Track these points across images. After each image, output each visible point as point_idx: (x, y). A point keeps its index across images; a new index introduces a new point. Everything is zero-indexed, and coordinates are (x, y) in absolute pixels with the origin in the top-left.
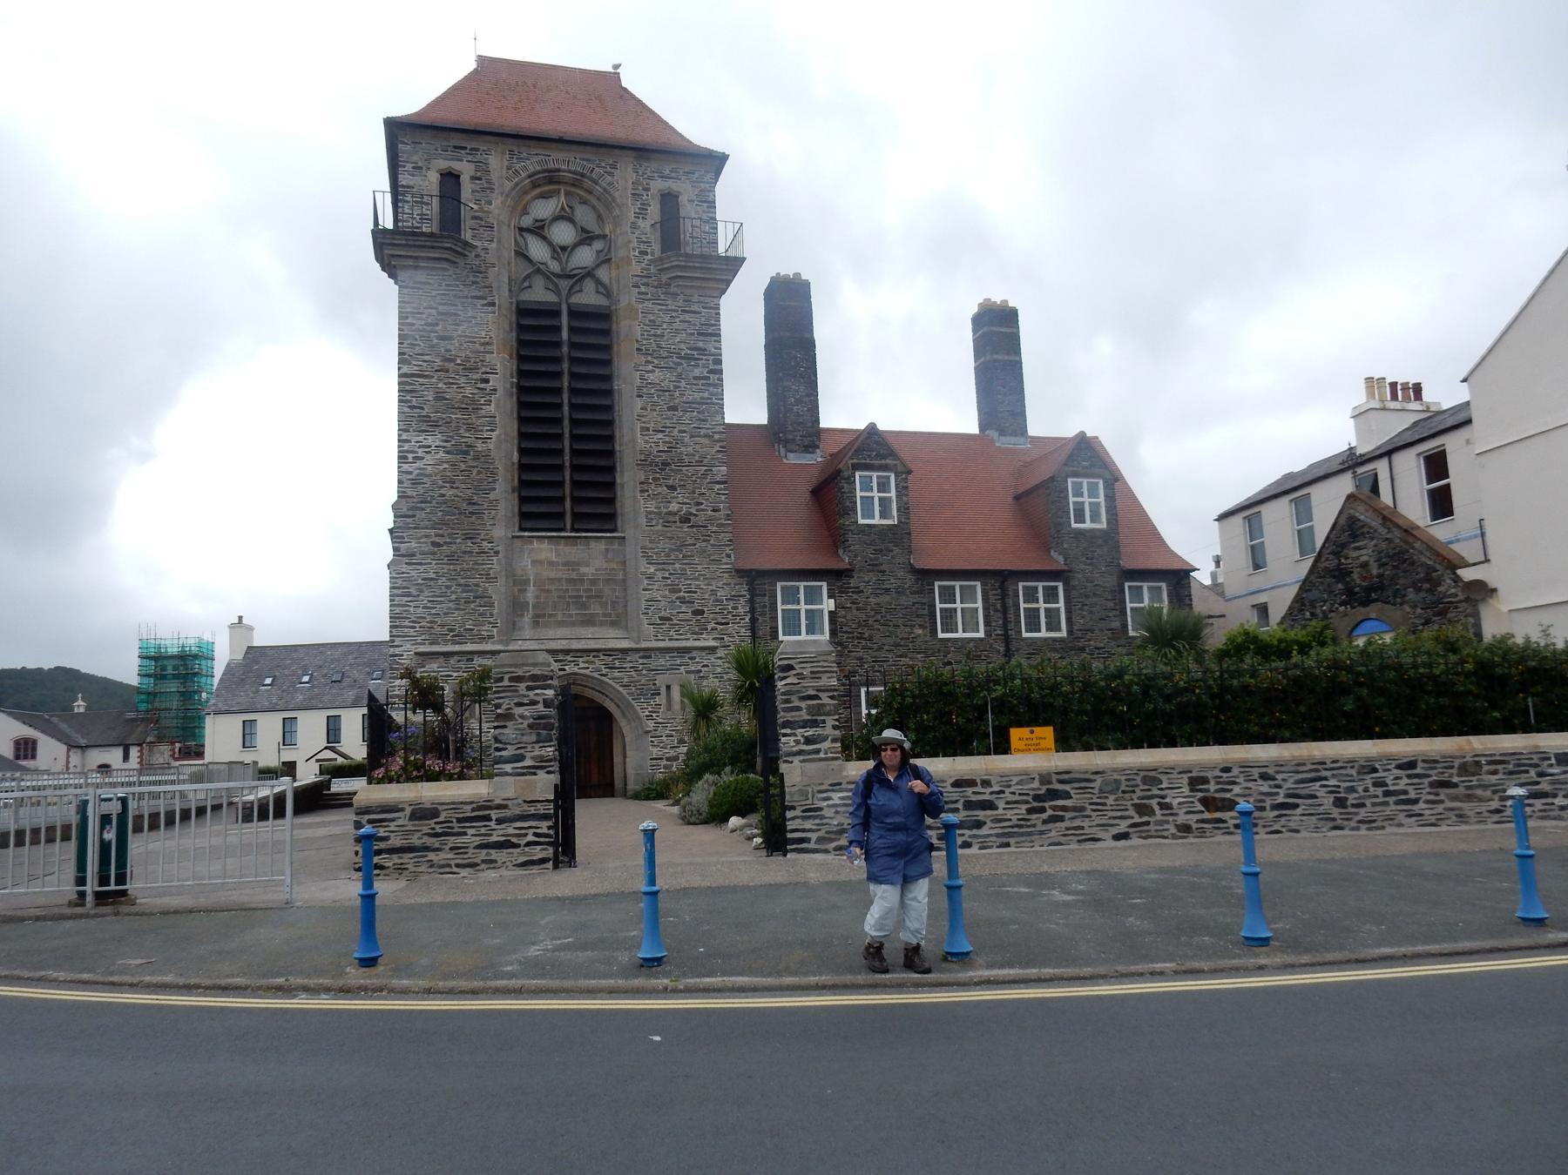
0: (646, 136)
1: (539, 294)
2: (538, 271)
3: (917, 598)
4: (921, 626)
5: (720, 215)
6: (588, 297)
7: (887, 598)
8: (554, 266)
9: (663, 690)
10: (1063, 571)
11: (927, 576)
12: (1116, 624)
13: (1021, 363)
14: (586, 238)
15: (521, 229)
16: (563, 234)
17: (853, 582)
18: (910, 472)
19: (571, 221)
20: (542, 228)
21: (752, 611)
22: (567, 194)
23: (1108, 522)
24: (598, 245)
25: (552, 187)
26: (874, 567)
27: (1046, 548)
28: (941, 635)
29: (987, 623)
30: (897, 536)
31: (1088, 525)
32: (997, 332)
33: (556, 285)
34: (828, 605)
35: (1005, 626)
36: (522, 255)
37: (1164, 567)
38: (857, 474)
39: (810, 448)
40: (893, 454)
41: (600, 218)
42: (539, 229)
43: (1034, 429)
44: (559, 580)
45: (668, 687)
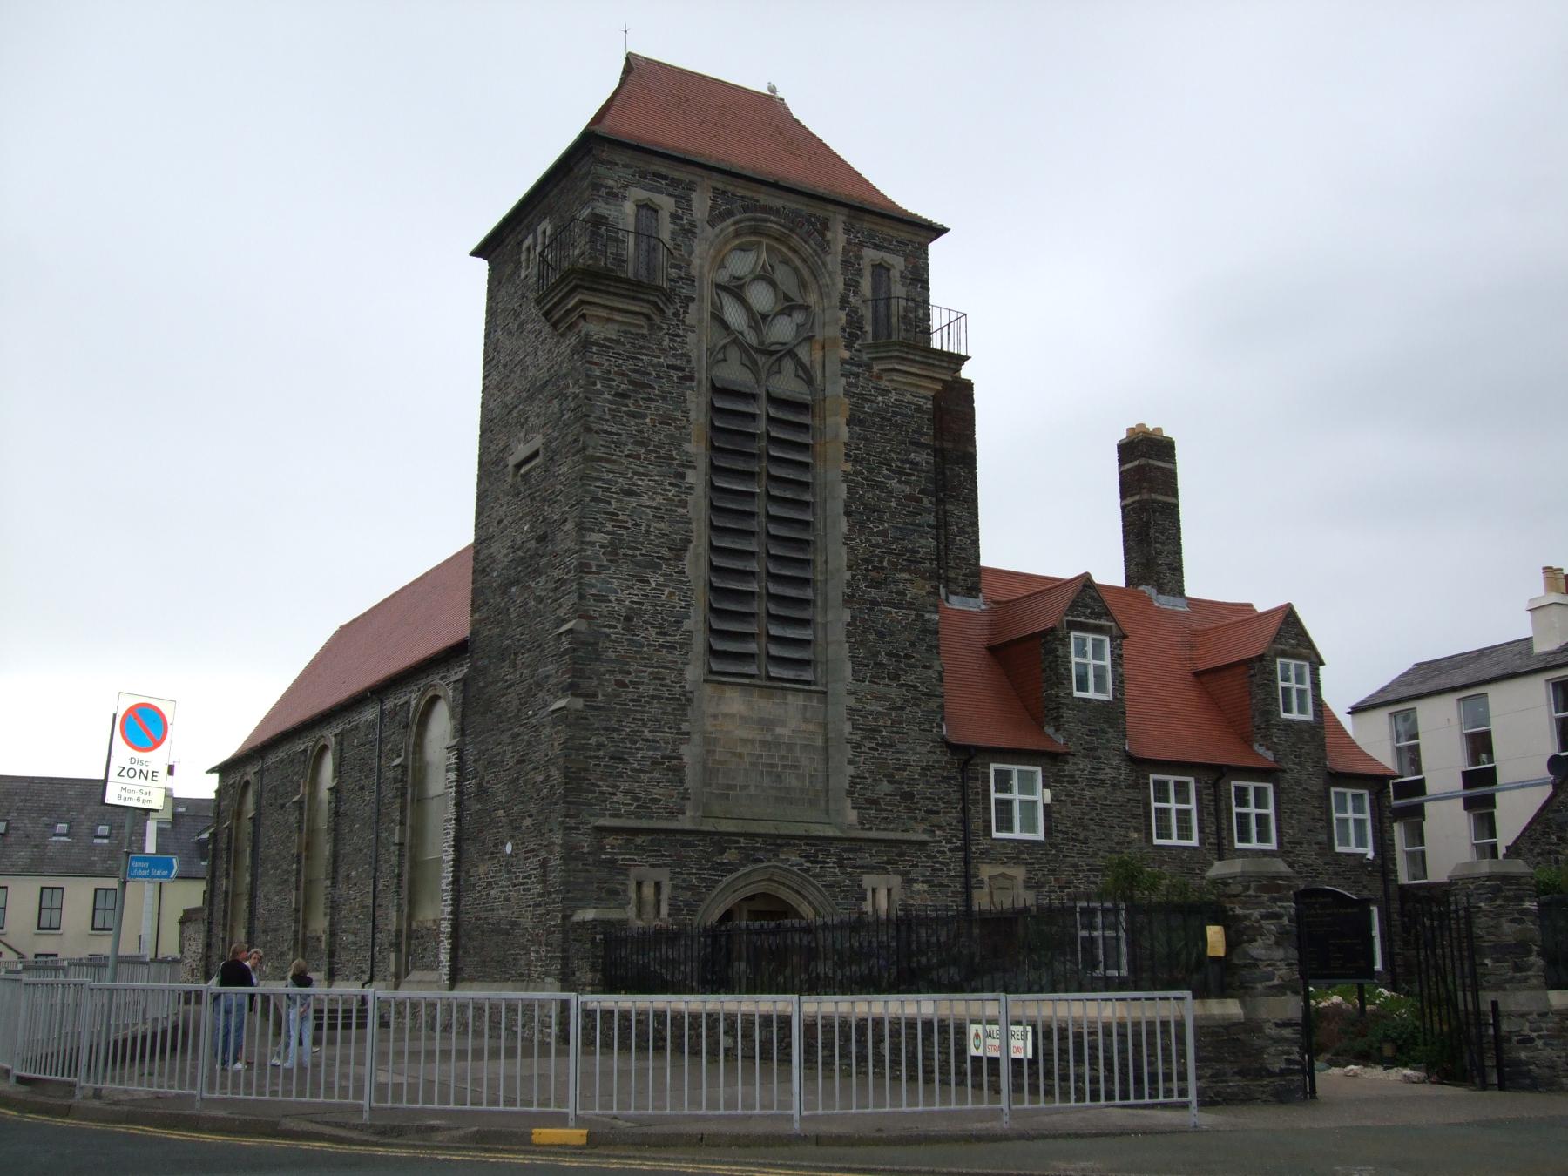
0: (844, 191)
1: (734, 372)
2: (735, 341)
3: (1132, 794)
4: (1137, 830)
5: (935, 298)
6: (787, 384)
7: (1102, 792)
8: (751, 337)
9: (869, 894)
10: (1276, 770)
11: (1143, 765)
12: (1323, 837)
13: (1176, 506)
14: (789, 306)
15: (718, 286)
16: (762, 298)
17: (1069, 769)
18: (1125, 637)
19: (773, 284)
20: (741, 287)
21: (964, 798)
22: (770, 249)
23: (1315, 715)
24: (799, 317)
25: (753, 238)
26: (1090, 752)
27: (1247, 741)
28: (995, 835)
29: (1201, 830)
30: (1110, 715)
31: (1091, 694)
32: (1147, 468)
33: (755, 362)
34: (1043, 796)
35: (1219, 829)
36: (719, 319)
37: (1339, 769)
38: (1073, 634)
39: (972, 591)
40: (1107, 614)
41: (803, 285)
42: (736, 290)
43: (1191, 590)
44: (752, 741)
45: (874, 890)
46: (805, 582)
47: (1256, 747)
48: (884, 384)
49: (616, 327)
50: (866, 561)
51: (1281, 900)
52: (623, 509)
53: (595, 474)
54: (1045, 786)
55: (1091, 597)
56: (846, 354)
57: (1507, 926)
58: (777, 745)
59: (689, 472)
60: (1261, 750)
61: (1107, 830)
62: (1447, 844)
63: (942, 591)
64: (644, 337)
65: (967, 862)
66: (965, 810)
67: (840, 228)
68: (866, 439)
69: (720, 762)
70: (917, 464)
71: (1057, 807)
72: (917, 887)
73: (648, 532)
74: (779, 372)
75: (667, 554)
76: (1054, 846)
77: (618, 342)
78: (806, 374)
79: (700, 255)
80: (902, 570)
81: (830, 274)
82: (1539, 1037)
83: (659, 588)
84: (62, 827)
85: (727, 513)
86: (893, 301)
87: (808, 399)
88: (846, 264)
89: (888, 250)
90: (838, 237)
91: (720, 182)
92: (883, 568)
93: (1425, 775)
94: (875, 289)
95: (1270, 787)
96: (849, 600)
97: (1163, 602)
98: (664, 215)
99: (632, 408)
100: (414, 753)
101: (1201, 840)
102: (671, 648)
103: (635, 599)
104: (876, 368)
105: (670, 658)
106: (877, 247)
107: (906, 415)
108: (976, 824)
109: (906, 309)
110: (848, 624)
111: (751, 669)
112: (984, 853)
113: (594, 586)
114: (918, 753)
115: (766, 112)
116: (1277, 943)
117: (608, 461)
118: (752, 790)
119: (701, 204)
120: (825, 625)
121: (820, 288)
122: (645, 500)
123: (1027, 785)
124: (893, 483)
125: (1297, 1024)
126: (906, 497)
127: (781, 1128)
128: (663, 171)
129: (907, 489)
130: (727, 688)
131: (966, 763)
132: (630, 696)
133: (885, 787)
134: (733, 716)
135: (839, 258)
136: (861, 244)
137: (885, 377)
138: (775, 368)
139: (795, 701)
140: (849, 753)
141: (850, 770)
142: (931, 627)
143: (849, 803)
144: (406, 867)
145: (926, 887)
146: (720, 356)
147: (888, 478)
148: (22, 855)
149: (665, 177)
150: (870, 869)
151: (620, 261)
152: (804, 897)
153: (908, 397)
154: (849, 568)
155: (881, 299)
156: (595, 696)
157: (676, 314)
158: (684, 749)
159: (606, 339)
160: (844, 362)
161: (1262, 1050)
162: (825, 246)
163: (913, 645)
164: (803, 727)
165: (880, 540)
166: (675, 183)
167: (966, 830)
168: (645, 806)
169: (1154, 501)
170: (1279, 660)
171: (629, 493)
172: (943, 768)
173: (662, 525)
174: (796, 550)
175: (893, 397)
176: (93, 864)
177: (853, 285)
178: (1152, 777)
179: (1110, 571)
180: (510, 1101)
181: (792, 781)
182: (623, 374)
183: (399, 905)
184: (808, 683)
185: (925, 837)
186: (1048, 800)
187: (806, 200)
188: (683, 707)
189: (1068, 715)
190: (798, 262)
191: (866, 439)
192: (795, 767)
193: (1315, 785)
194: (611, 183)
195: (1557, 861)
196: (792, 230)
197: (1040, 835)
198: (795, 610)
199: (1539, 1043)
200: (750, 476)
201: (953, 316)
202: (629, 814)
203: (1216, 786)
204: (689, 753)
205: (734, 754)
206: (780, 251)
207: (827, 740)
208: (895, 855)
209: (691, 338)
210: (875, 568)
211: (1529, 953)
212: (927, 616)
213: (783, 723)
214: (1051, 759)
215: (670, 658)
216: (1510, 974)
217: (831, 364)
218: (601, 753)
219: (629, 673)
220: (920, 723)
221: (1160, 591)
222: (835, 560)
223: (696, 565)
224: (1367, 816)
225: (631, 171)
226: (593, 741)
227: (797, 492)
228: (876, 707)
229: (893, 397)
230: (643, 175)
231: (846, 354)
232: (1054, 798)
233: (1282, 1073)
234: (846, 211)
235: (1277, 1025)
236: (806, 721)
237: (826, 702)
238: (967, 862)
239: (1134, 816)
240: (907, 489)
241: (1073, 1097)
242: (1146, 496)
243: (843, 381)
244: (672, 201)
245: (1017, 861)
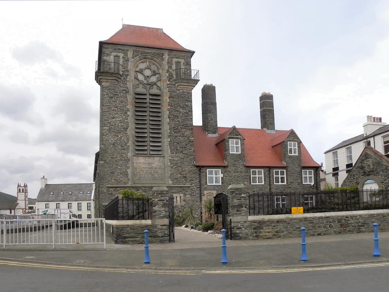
0: (179, 48)
1: (141, 90)
6: (154, 91)
7: (238, 174)
14: (154, 74)
15: (136, 71)
16: (148, 73)
18: (245, 139)
20: (142, 71)
21: (200, 177)
24: (157, 76)
26: (234, 165)
29: (265, 181)
30: (241, 157)
31: (293, 154)
33: (146, 87)
36: (136, 78)
39: (214, 133)
40: (240, 135)
41: (158, 69)
43: (276, 128)
44: (146, 168)
45: (176, 197)
46: (160, 133)
48: (178, 88)
49: (109, 83)
50: (174, 127)
51: (164, 196)
52: (112, 122)
53: (105, 115)
55: (235, 131)
56: (169, 83)
57: (235, 201)
58: (152, 168)
59: (128, 112)
61: (239, 182)
62: (330, 182)
63: (207, 133)
64: (116, 84)
65: (200, 190)
66: (200, 179)
67: (167, 55)
68: (174, 101)
69: (138, 172)
70: (188, 105)
71: (225, 177)
72: (187, 196)
73: (118, 126)
74: (153, 88)
75: (123, 130)
77: (110, 86)
78: (159, 88)
79: (130, 66)
80: (183, 129)
81: (164, 65)
82: (243, 227)
83: (121, 138)
84: (81, 192)
85: (139, 121)
86: (181, 69)
87: (160, 94)
88: (168, 63)
89: (179, 58)
90: (166, 57)
91: (135, 49)
92: (178, 129)
93: (339, 166)
94: (176, 67)
95: (285, 171)
96: (169, 136)
97: (268, 131)
98: (121, 58)
99: (114, 100)
102: (124, 149)
103: (115, 140)
104: (176, 85)
105: (124, 152)
107: (185, 95)
108: (203, 182)
109: (184, 71)
110: (169, 142)
111: (146, 153)
113: (105, 138)
114: (188, 168)
115: (158, 33)
116: (162, 207)
117: (108, 112)
118: (146, 178)
119: (130, 54)
120: (164, 142)
121: (162, 69)
122: (117, 119)
123: (260, 173)
124: (181, 110)
125: (167, 225)
126: (184, 113)
127: (48, 248)
128: (121, 48)
129: (185, 111)
130: (139, 157)
131: (200, 169)
132: (115, 160)
133: (179, 175)
134: (141, 163)
135: (167, 61)
136: (173, 58)
137: (179, 87)
138: (151, 88)
139: (157, 159)
140: (170, 168)
141: (170, 172)
142: (191, 141)
143: (170, 179)
145: (190, 196)
146: (137, 86)
147: (180, 109)
148: (74, 198)
149: (121, 49)
150: (175, 193)
151: (110, 69)
153: (185, 90)
154: (169, 129)
155: (178, 69)
156: (106, 160)
157: (124, 79)
158: (128, 170)
159: (107, 86)
160: (168, 84)
161: (156, 231)
162: (163, 60)
163: (186, 145)
164: (159, 164)
165: (178, 123)
166: (124, 50)
167: (200, 184)
168: (119, 182)
169: (267, 109)
170: (288, 142)
171: (113, 118)
172: (194, 171)
173: (122, 124)
174: (157, 126)
175: (181, 91)
176: (86, 198)
177: (170, 67)
179: (257, 125)
180: (56, 241)
181: (156, 175)
182: (111, 93)
184: (160, 155)
185: (190, 186)
187: (157, 50)
188: (127, 162)
189: (228, 158)
190: (156, 64)
191: (174, 101)
192: (157, 172)
194: (107, 52)
195: (353, 183)
196: (154, 57)
198: (157, 139)
199: (243, 229)
200: (146, 111)
201: (197, 71)
202: (115, 184)
203: (269, 171)
204: (129, 171)
205: (142, 171)
208: (182, 189)
209: (128, 83)
210: (176, 129)
211: (242, 207)
212: (190, 138)
213: (154, 164)
215: (124, 152)
216: (236, 212)
217: (164, 85)
218: (108, 172)
219: (114, 155)
220: (188, 162)
221: (268, 129)
222: (166, 128)
223: (131, 132)
225: (112, 49)
226: (106, 170)
227: (157, 114)
228: (176, 159)
229: (181, 91)
230: (115, 50)
231: (169, 83)
233: (162, 237)
234: (168, 51)
235: (161, 226)
236: (160, 163)
238: (200, 190)
239: (246, 179)
240: (185, 111)
241: (52, 243)
242: (264, 108)
243: (168, 88)
244: (123, 54)
245: (214, 190)
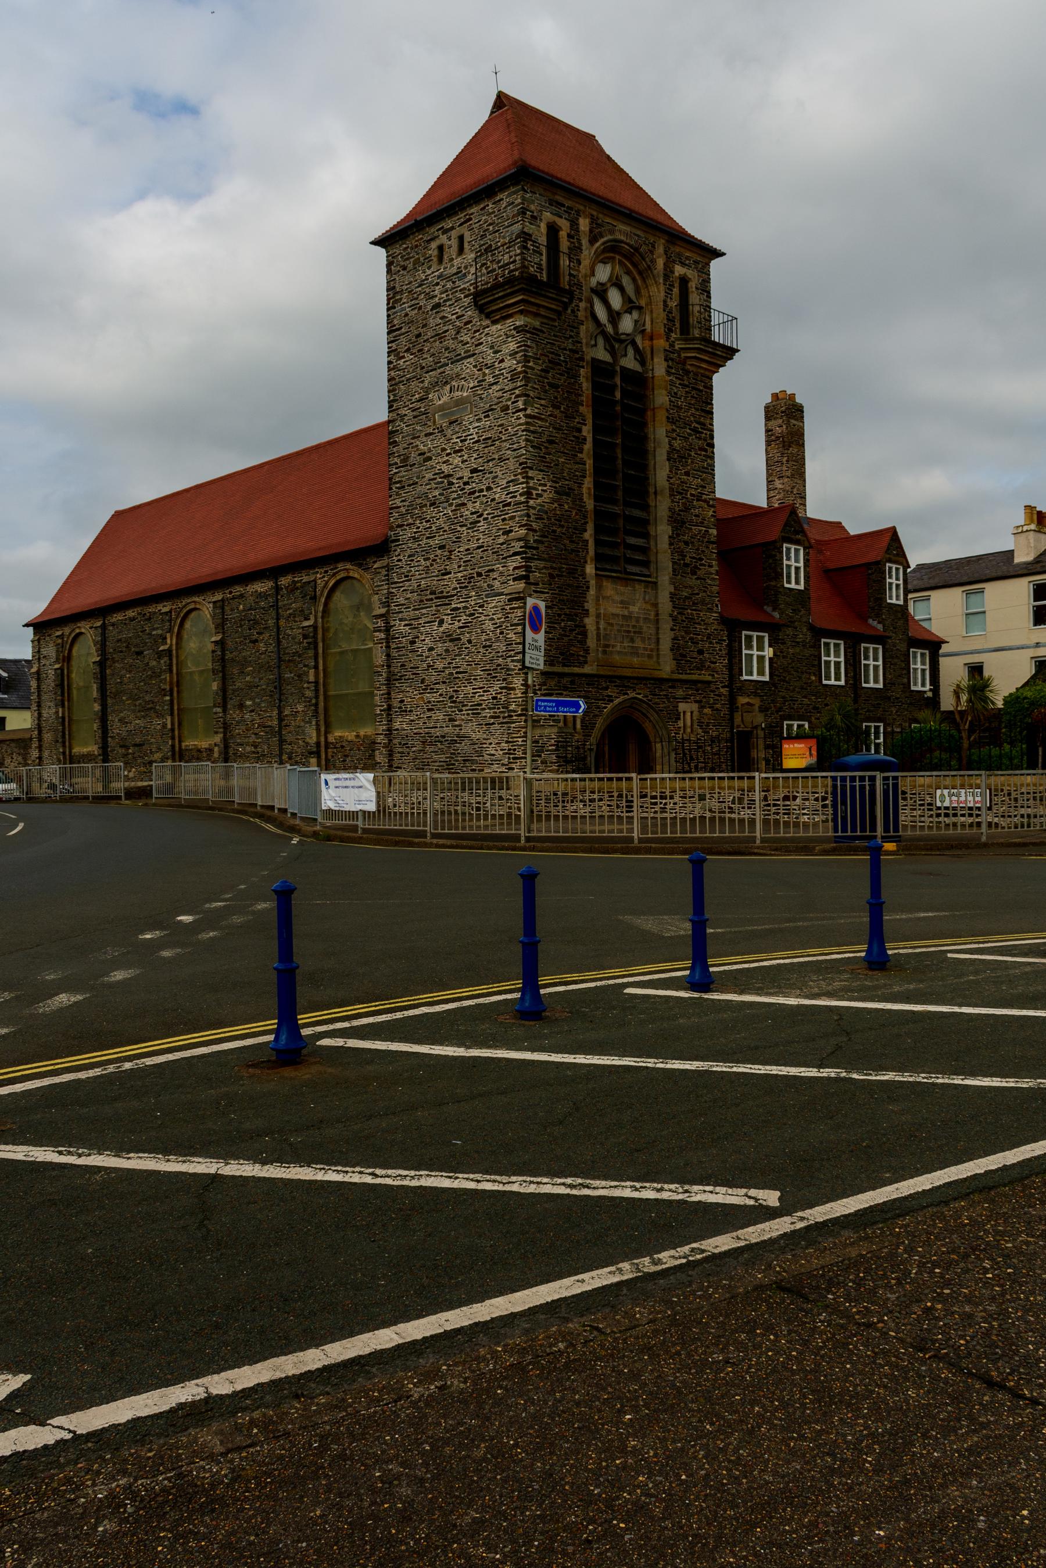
0: (627, 200)
4: (815, 675)
6: (629, 362)
7: (798, 650)
14: (630, 306)
29: (846, 676)
33: (612, 347)
34: (768, 652)
42: (601, 292)
44: (618, 615)
47: (870, 621)
54: (770, 646)
60: (875, 623)
76: (774, 685)
100: (323, 617)
101: (846, 681)
106: (683, 264)
112: (740, 689)
144: (321, 698)
152: (647, 717)
178: (823, 640)
183: (317, 725)
185: (710, 678)
186: (771, 655)
193: (902, 647)
197: (767, 678)
206: (625, 265)
207: (657, 615)
214: (773, 629)
224: (927, 667)
232: (775, 654)
237: (656, 589)
